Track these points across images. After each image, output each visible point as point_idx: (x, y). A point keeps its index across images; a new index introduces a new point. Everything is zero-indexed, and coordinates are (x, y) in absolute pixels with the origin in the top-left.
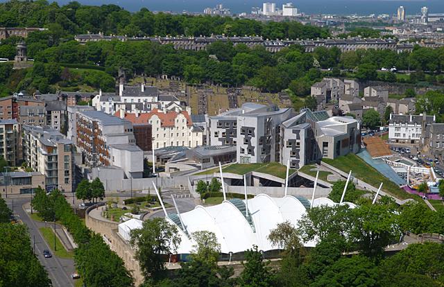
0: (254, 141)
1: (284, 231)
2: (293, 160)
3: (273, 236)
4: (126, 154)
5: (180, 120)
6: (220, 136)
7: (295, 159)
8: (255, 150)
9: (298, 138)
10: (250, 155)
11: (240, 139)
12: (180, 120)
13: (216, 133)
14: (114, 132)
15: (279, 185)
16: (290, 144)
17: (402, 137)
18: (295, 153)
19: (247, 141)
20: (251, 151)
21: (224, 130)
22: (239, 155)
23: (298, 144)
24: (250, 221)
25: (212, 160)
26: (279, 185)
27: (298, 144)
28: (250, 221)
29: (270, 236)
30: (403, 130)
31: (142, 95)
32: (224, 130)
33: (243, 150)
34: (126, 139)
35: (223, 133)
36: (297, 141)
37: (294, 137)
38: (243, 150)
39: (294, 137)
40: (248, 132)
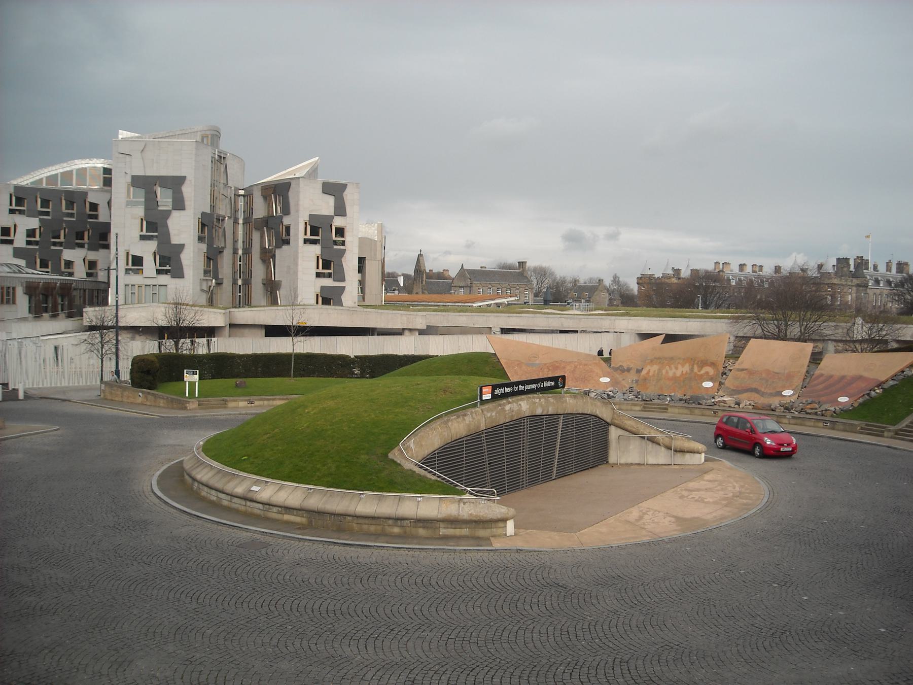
2: (322, 288)
7: (328, 282)
10: (164, 279)
16: (314, 231)
33: (137, 261)
35: (31, 233)
36: (338, 222)
38: (137, 261)
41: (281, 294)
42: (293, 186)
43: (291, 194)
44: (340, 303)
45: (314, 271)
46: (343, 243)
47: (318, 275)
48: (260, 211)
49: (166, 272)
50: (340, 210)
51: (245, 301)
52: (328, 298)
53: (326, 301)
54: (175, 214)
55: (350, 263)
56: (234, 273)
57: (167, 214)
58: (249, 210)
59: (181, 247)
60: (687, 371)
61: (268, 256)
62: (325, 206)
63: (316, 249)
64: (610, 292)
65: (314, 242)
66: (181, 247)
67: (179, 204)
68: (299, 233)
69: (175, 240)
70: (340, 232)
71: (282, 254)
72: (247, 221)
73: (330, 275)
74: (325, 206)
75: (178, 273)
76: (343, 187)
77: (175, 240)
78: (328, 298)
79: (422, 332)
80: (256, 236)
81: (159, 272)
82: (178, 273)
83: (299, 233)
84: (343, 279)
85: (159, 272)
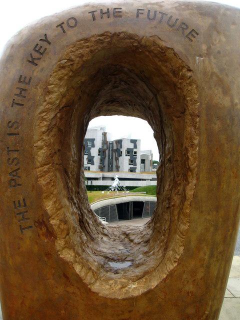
7: (132, 166)
10: (89, 165)
16: (128, 152)
36: (135, 150)
41: (120, 169)
42: (123, 141)
43: (122, 143)
44: (135, 172)
45: (128, 163)
46: (136, 156)
47: (129, 164)
48: (115, 148)
49: (90, 163)
50: (135, 147)
51: (110, 170)
52: (132, 170)
53: (131, 171)
54: (92, 148)
55: (138, 161)
56: (109, 164)
57: (90, 149)
58: (113, 147)
59: (94, 157)
60: (163, 6)
61: (117, 159)
62: (131, 146)
63: (129, 157)
64: (155, 224)
65: (129, 155)
66: (94, 157)
67: (93, 146)
68: (124, 153)
69: (92, 155)
70: (135, 153)
71: (120, 158)
72: (112, 150)
73: (132, 164)
74: (131, 146)
75: (93, 164)
76: (136, 141)
77: (92, 155)
78: (132, 170)
79: (151, 180)
80: (114, 154)
81: (88, 163)
82: (93, 164)
83: (124, 153)
84: (136, 165)
85: (88, 163)
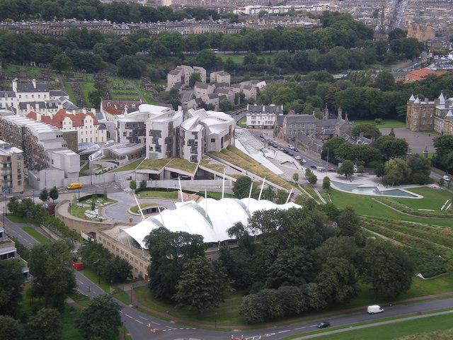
0: (161, 141)
1: (237, 228)
3: (231, 231)
4: (59, 164)
5: (88, 121)
6: (128, 135)
8: (162, 148)
9: (196, 138)
11: (149, 139)
12: (88, 121)
13: (124, 133)
14: (166, 197)
15: (189, 178)
17: (257, 124)
18: (194, 150)
19: (155, 141)
20: (158, 149)
21: (131, 131)
22: (148, 151)
23: (197, 143)
24: (208, 219)
25: (127, 158)
26: (189, 178)
27: (197, 143)
28: (211, 224)
29: (230, 230)
30: (258, 119)
31: (36, 91)
32: (131, 131)
33: (152, 148)
34: (59, 145)
36: (196, 141)
37: (193, 137)
39: (193, 137)
40: (156, 134)
75: (160, 151)
82: (160, 151)
